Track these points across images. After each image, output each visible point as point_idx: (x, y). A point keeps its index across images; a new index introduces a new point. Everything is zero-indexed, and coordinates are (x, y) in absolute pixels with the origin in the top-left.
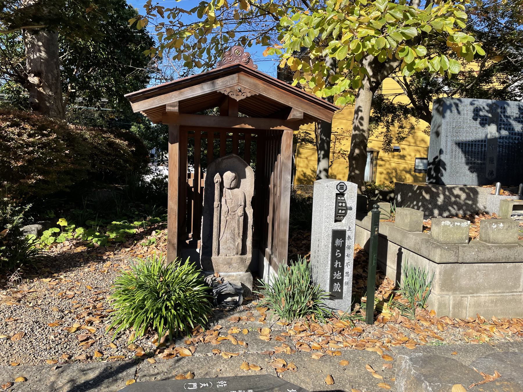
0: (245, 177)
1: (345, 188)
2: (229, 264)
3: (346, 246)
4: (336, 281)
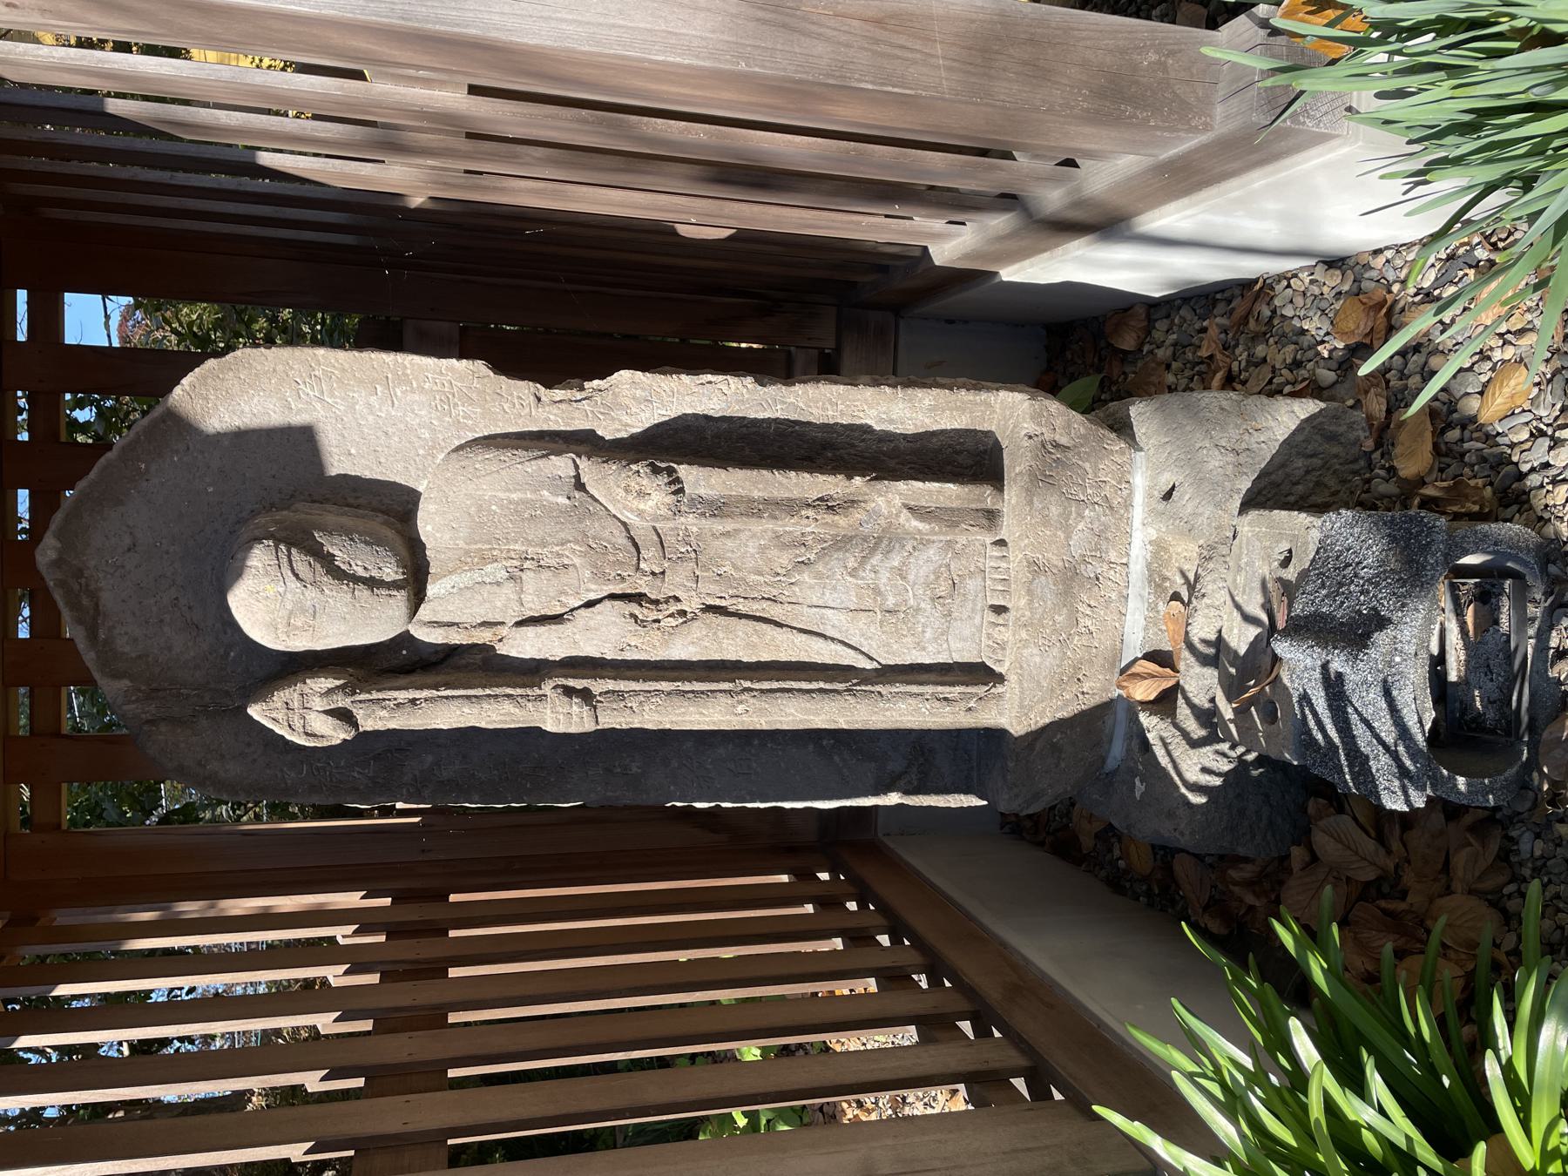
0: (302, 441)
2: (1071, 579)
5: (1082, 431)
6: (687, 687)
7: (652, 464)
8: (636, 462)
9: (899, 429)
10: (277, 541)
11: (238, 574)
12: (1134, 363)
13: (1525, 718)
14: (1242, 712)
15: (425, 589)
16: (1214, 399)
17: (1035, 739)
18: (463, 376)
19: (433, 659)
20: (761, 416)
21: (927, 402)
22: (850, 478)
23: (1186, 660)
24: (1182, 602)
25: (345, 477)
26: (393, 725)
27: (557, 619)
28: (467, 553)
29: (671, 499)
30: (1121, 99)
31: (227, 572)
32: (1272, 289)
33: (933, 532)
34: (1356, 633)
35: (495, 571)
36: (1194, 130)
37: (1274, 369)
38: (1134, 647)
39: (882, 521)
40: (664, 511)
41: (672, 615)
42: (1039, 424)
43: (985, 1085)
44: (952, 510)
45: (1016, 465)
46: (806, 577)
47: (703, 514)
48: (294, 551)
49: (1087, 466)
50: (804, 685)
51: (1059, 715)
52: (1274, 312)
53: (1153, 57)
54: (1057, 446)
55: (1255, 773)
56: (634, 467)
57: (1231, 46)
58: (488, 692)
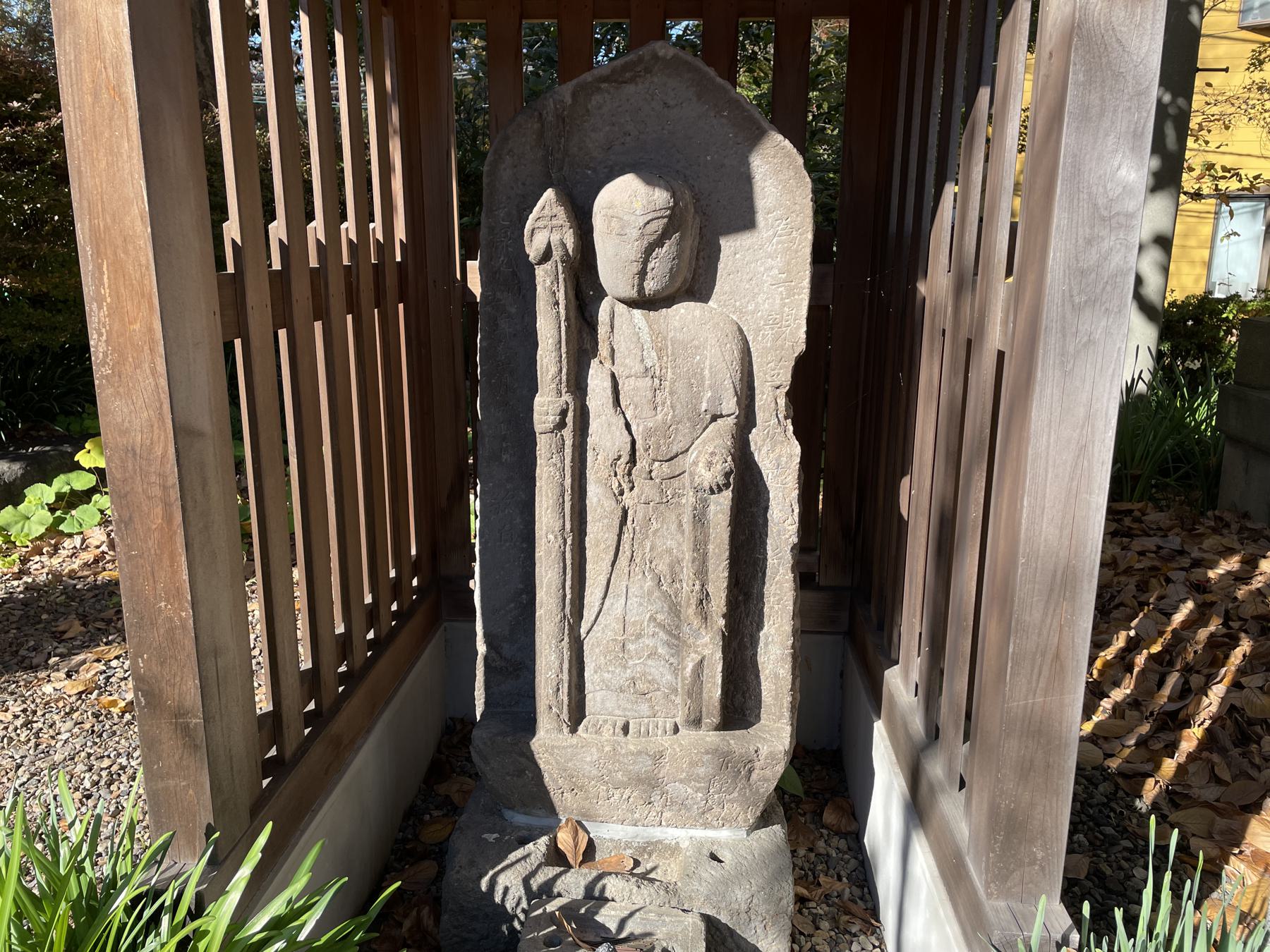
0: (745, 220)
2: (649, 784)
5: (762, 790)
6: (567, 498)
8: (733, 460)
10: (672, 209)
11: (649, 182)
12: (813, 822)
15: (638, 308)
16: (787, 891)
17: (527, 758)
18: (796, 336)
19: (587, 314)
20: (769, 548)
21: (782, 671)
22: (724, 616)
23: (588, 874)
24: (633, 869)
25: (718, 250)
26: (539, 288)
27: (617, 402)
28: (665, 338)
29: (706, 485)
30: (1007, 831)
31: (651, 174)
32: (872, 934)
33: (684, 679)
35: (651, 359)
36: (987, 886)
37: (811, 936)
39: (691, 641)
41: (620, 485)
42: (766, 758)
43: (273, 724)
44: (701, 693)
45: (735, 740)
46: (649, 583)
47: (695, 509)
48: (666, 220)
49: (735, 794)
50: (568, 583)
51: (546, 775)
52: (855, 935)
53: (1040, 855)
54: (750, 771)
55: (504, 928)
56: (729, 459)
57: (1047, 913)
58: (564, 356)
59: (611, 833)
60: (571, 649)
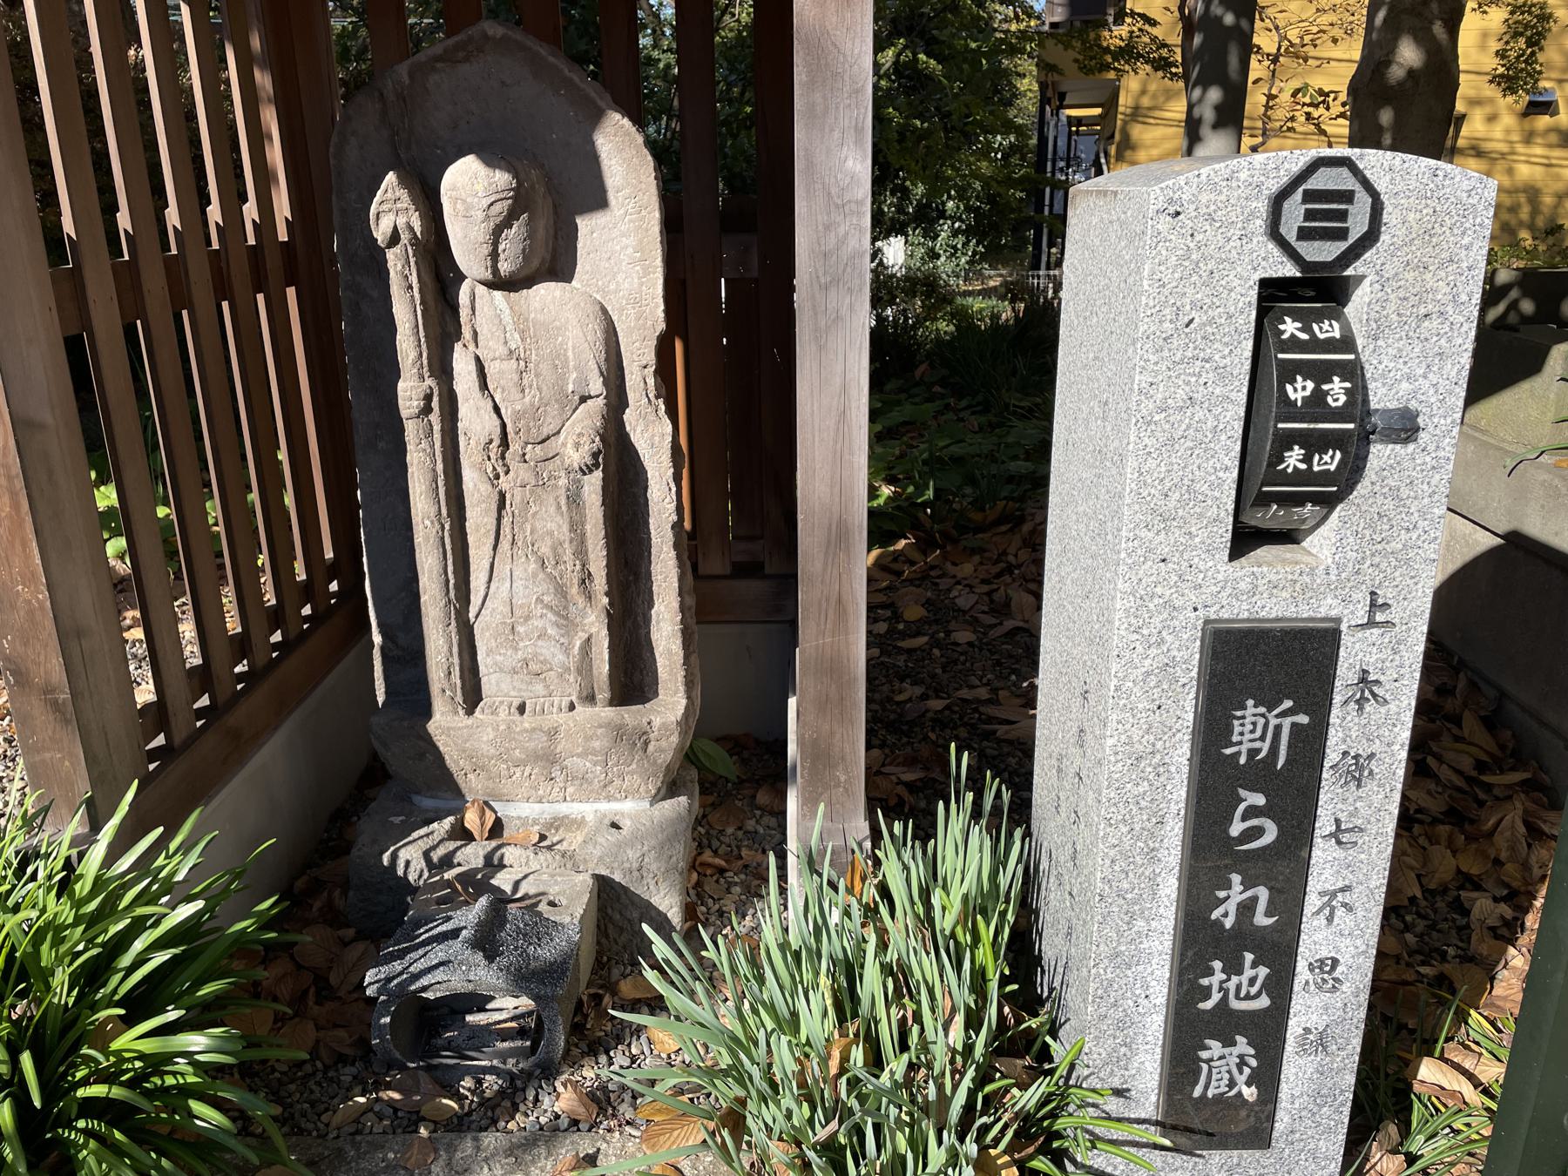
0: (599, 201)
1: (1357, 225)
2: (548, 760)
3: (1332, 756)
4: (1226, 1024)
6: (441, 483)
7: (600, 452)
9: (653, 629)
13: (436, 1061)
14: (449, 884)
22: (607, 594)
28: (527, 320)
34: (487, 942)
38: (502, 809)
40: (567, 462)
43: (157, 715)
45: (630, 715)
46: (533, 566)
49: (634, 766)
50: (450, 569)
53: (843, 779)
54: (646, 743)
59: (521, 812)
60: (459, 632)
